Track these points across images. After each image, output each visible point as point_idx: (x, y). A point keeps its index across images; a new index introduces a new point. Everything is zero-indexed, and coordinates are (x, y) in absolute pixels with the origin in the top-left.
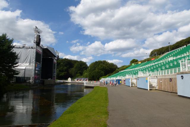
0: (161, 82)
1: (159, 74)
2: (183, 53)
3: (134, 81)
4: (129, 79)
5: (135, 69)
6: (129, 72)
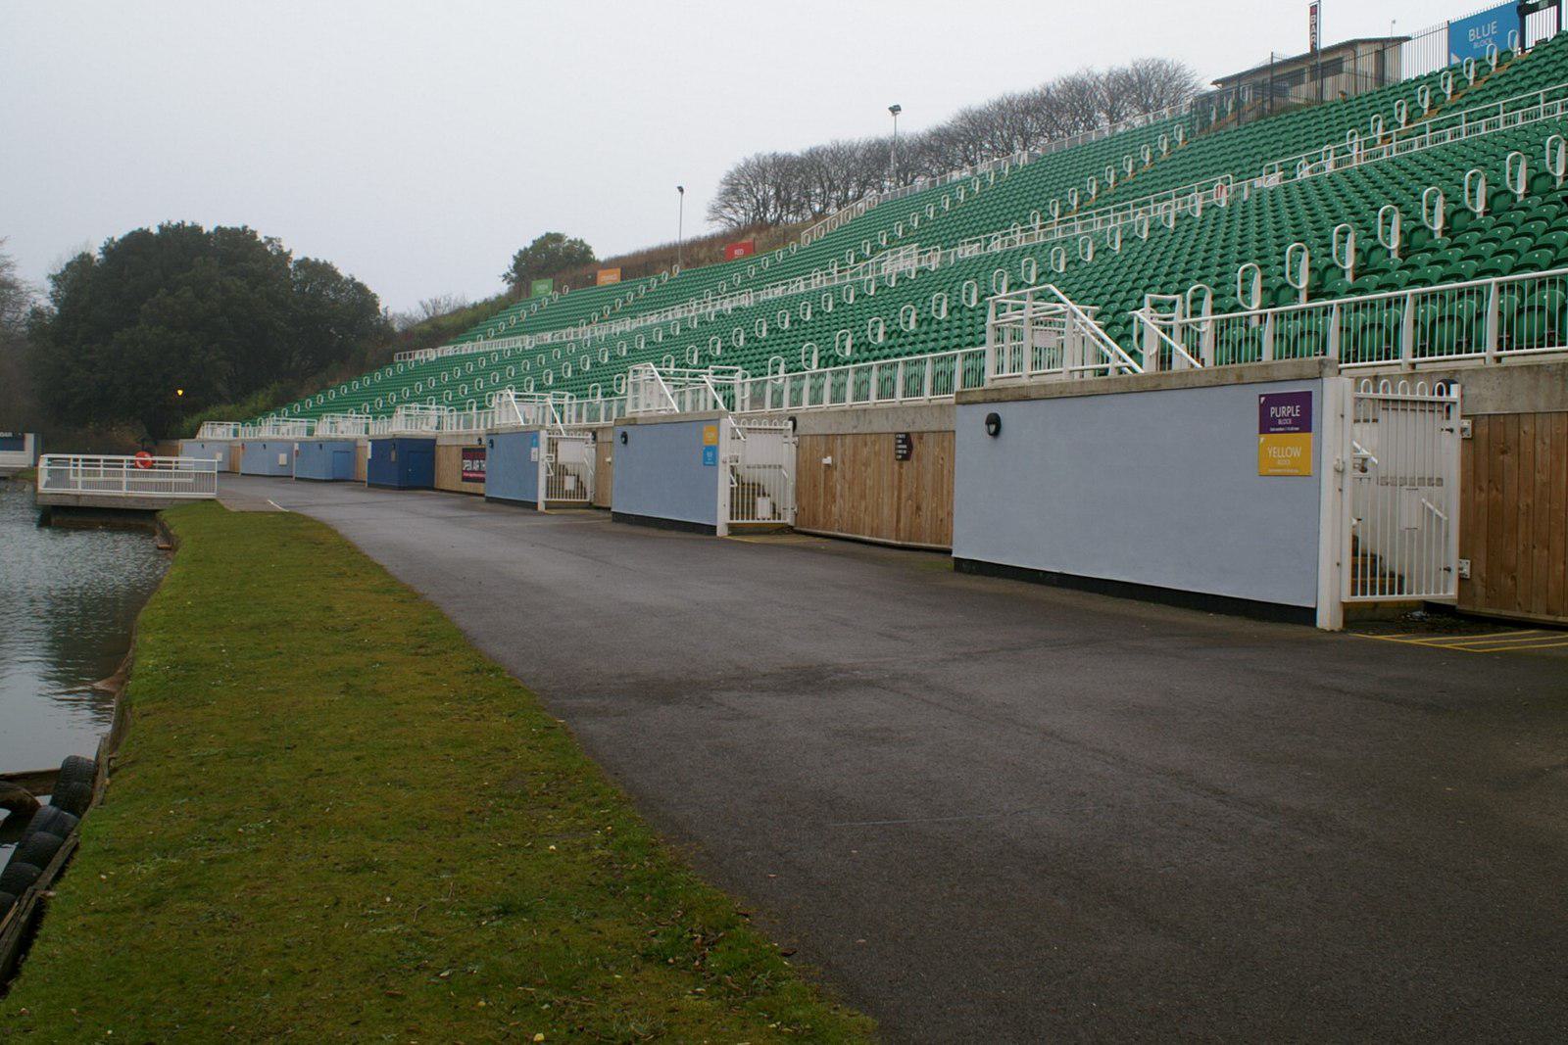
0: (828, 460)
1: (816, 399)
2: (1003, 225)
3: (577, 454)
4: (528, 436)
5: (568, 334)
6: (490, 368)
